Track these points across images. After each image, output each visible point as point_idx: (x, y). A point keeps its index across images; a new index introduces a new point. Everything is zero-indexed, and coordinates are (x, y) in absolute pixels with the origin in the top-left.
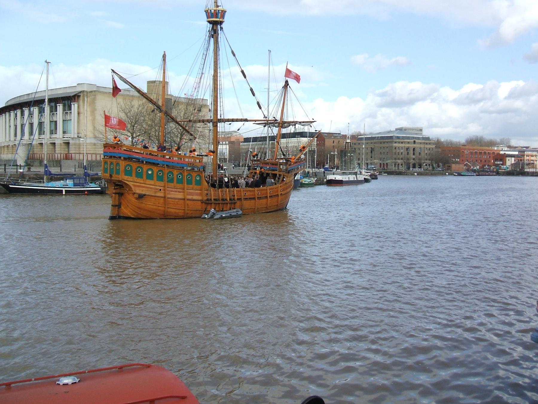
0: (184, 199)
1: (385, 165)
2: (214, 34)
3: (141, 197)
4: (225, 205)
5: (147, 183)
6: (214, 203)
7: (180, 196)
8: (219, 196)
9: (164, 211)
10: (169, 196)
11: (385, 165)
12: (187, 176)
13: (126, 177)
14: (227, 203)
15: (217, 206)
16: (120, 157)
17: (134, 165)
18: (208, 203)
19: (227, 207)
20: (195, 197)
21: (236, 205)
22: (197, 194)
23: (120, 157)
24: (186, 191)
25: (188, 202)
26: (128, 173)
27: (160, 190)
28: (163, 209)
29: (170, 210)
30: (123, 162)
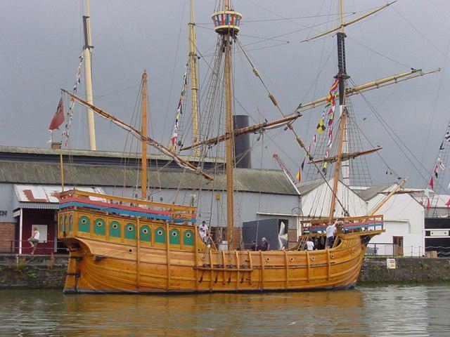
0: (285, 267)
1: (68, 218)
2: (224, 47)
3: (99, 259)
4: (220, 274)
5: (110, 241)
6: (241, 272)
7: (160, 259)
8: (223, 261)
9: (136, 280)
10: (143, 259)
11: (68, 218)
12: (170, 232)
13: (80, 234)
14: (237, 271)
15: (233, 275)
16: (73, 207)
17: (93, 217)
18: (219, 271)
19: (236, 277)
20: (183, 262)
21: (252, 274)
22: (187, 258)
23: (73, 207)
24: (169, 252)
25: (172, 268)
26: (84, 226)
27: (130, 251)
28: (134, 277)
29: (144, 279)
30: (77, 213)
